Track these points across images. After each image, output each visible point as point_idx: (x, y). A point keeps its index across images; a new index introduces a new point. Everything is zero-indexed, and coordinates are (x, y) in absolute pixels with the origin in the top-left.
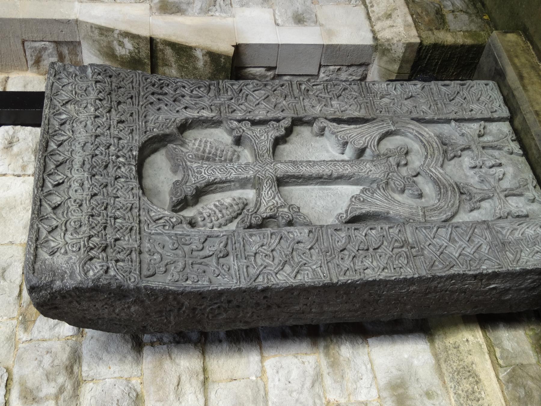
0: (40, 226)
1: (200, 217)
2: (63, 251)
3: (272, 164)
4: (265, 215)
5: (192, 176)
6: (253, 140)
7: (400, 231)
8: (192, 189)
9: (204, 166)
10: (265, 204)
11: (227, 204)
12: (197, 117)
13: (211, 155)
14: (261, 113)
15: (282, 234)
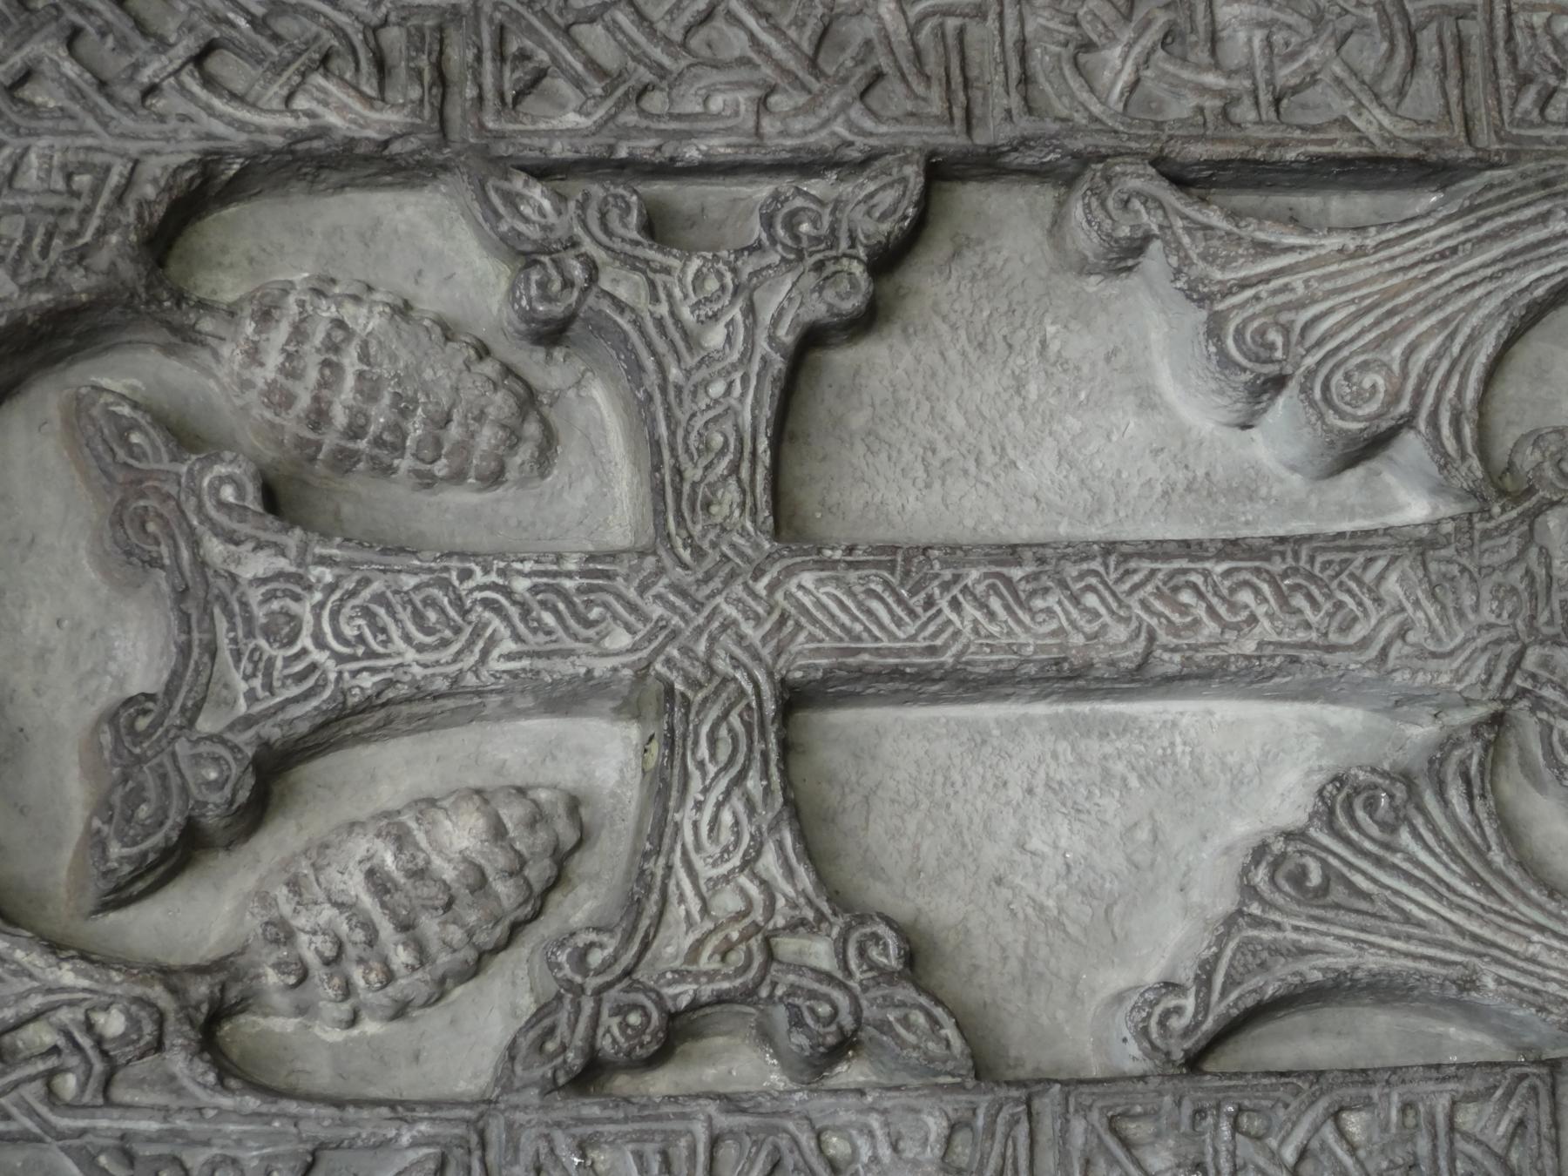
1: (279, 966)
3: (758, 573)
4: (682, 994)
5: (237, 656)
6: (649, 363)
7: (1521, 1124)
8: (235, 770)
9: (315, 572)
10: (695, 905)
11: (449, 874)
12: (277, 141)
13: (362, 444)
14: (716, 104)
15: (784, 1143)
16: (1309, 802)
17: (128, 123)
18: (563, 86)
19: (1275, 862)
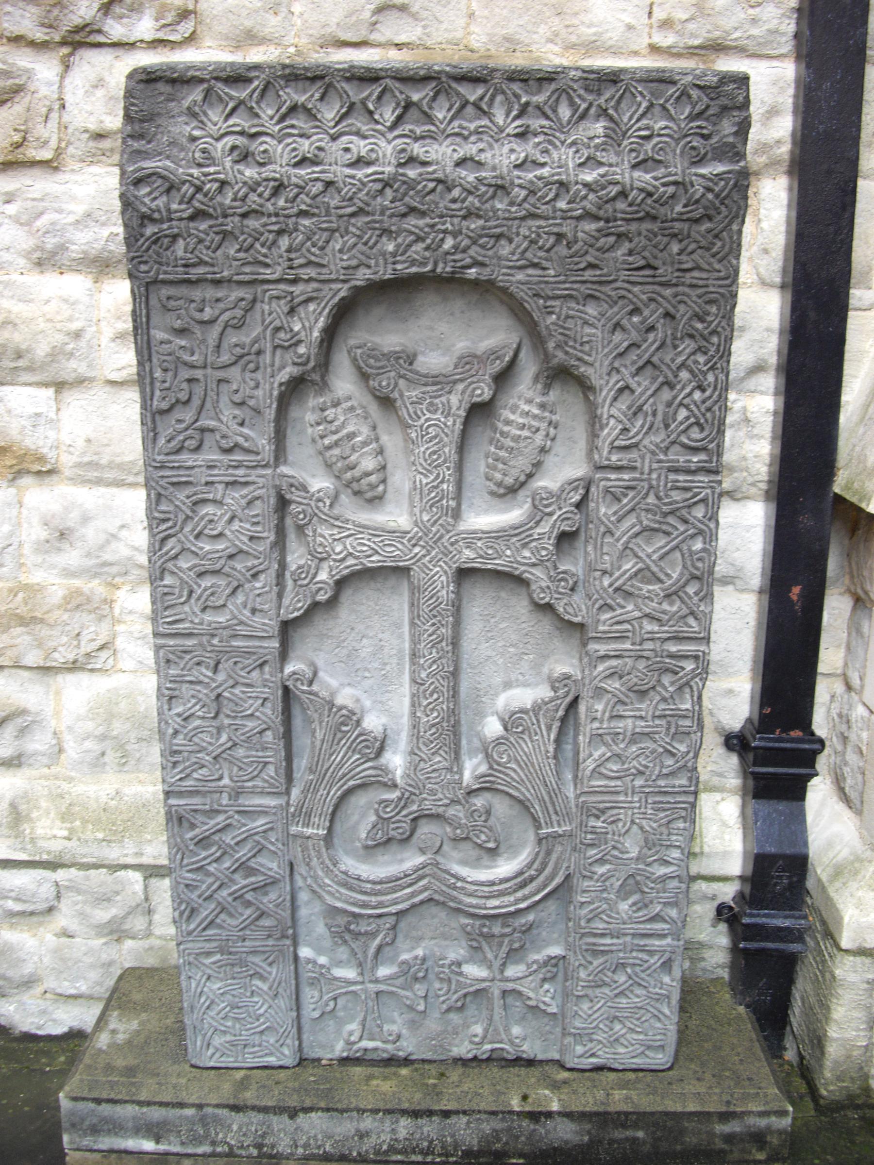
0: (256, 83)
2: (196, 133)
11: (352, 458)
16: (370, 728)
17: (606, 363)
18: (615, 508)
19: (351, 718)
